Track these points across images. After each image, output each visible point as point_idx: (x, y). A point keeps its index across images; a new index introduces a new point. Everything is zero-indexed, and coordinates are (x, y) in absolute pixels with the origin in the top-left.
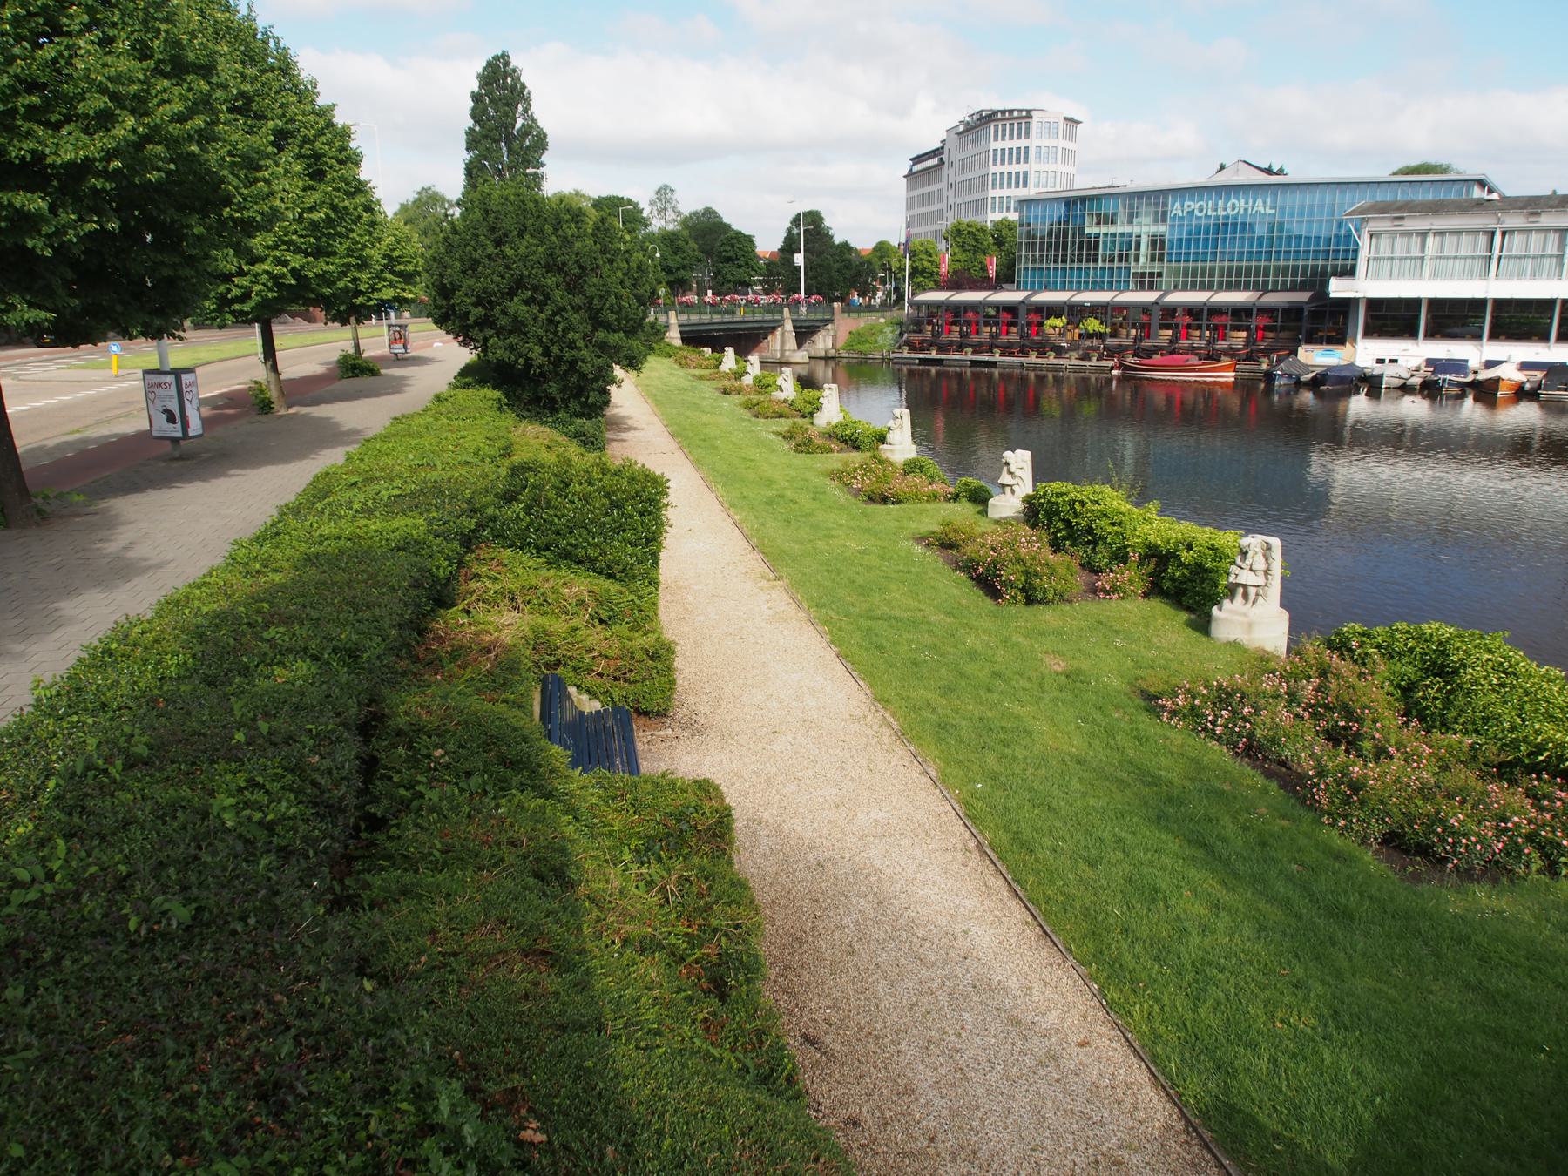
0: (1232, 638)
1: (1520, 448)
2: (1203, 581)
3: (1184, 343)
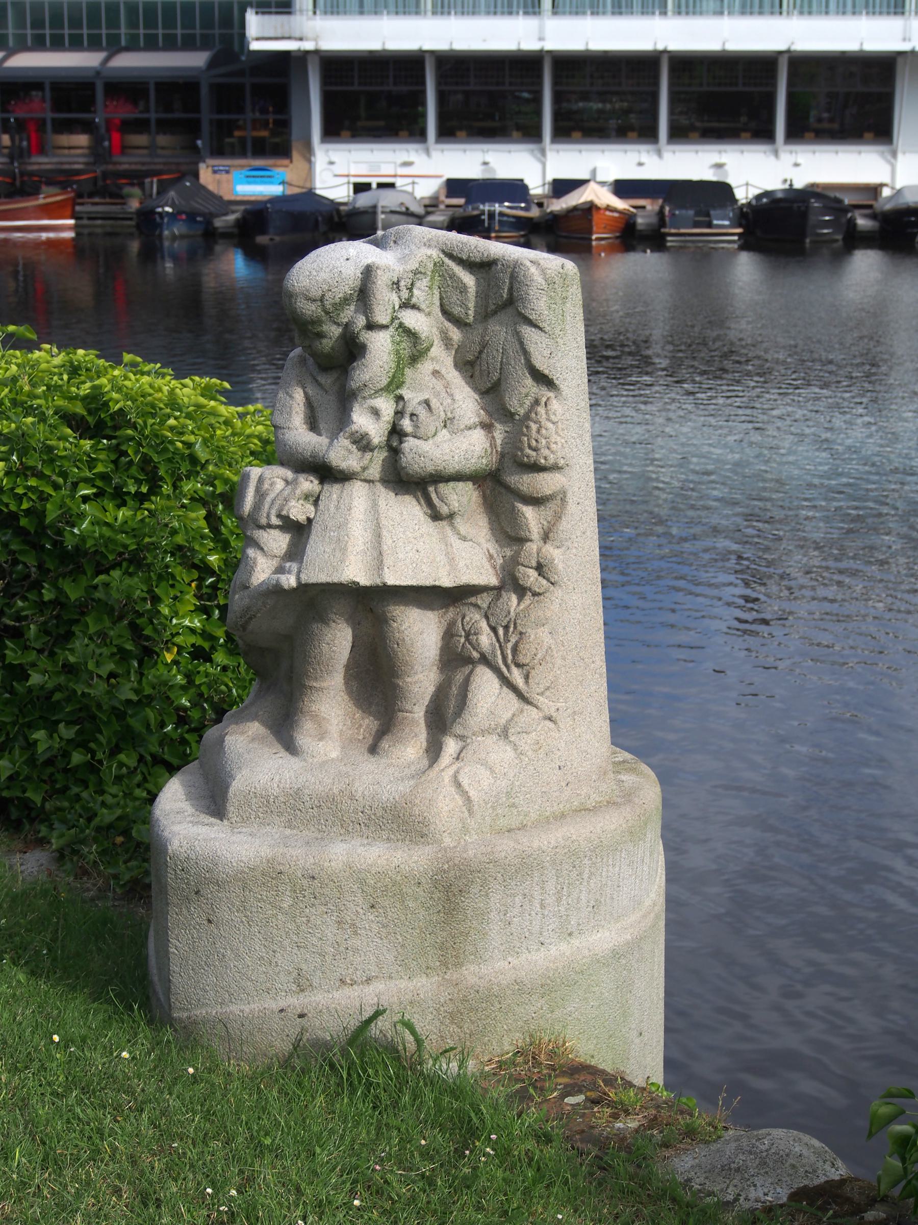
0: (335, 1005)
2: (62, 626)
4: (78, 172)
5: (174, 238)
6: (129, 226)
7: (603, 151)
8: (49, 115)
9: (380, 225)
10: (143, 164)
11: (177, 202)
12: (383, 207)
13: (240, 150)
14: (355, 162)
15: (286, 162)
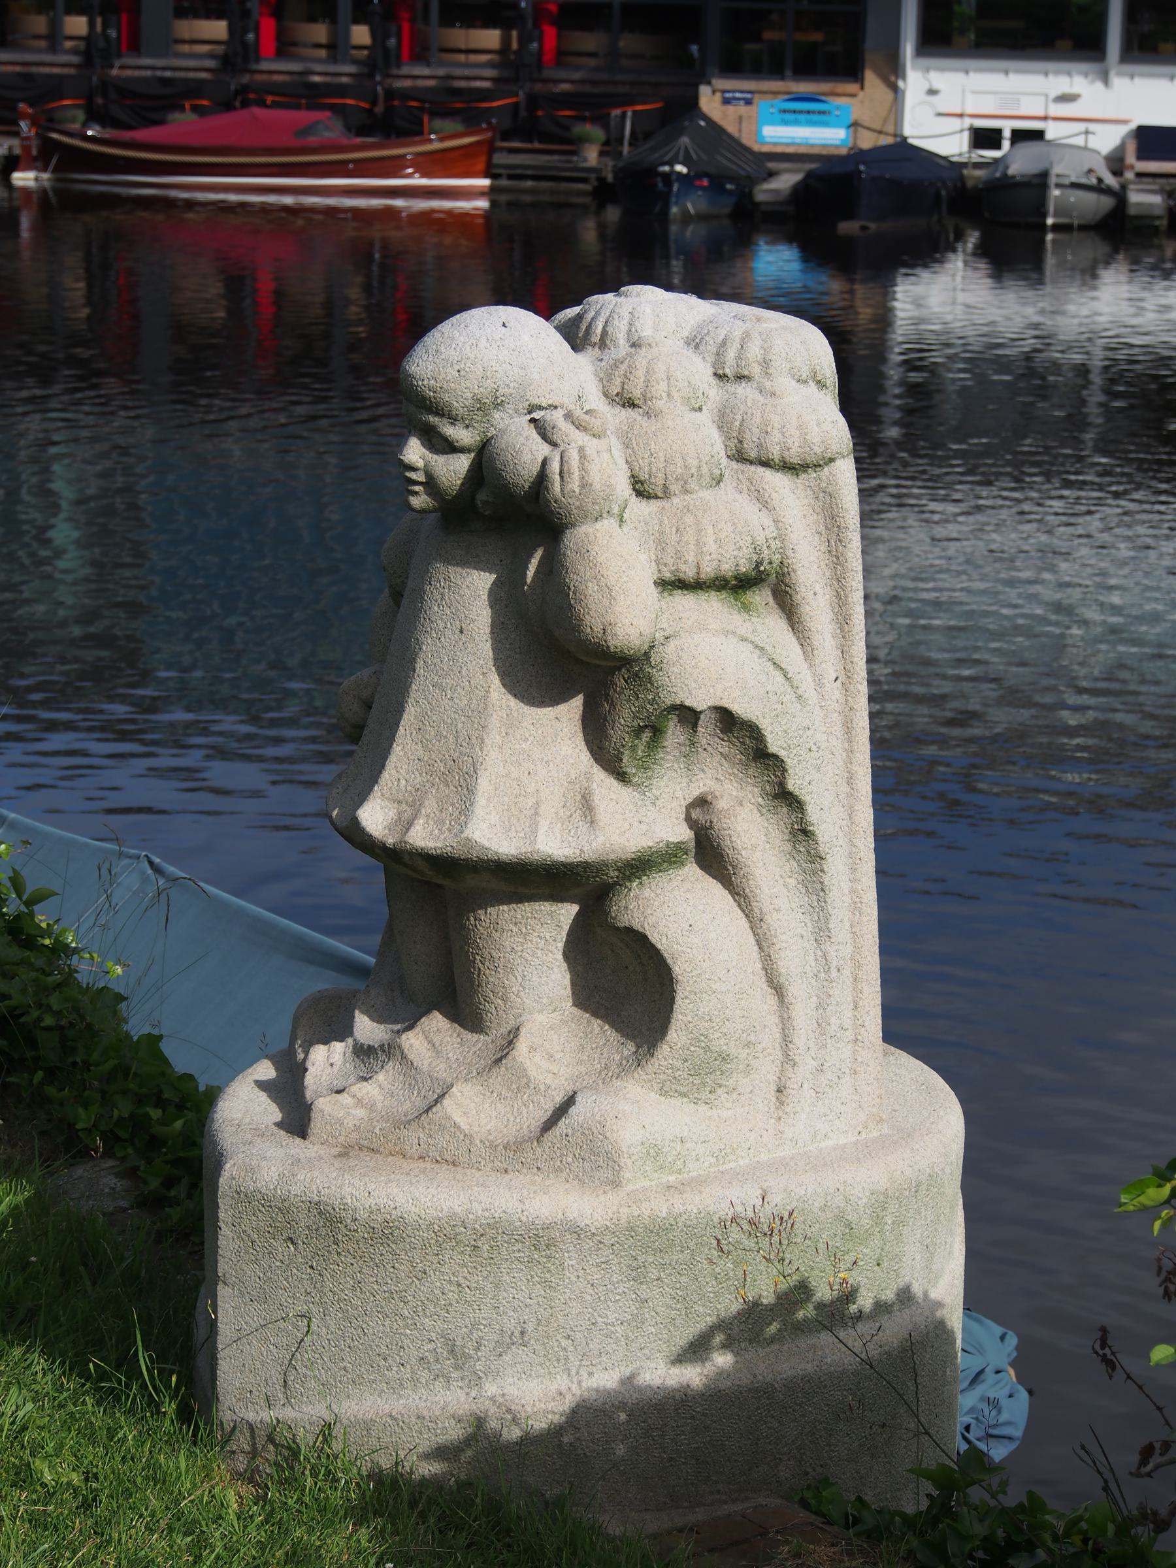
1: (961, 474)
3: (275, 68)
4: (485, 95)
5: (686, 219)
7: (1132, 77)
9: (1051, 209)
10: (594, 83)
11: (694, 157)
12: (1058, 176)
14: (974, 92)
15: (852, 87)
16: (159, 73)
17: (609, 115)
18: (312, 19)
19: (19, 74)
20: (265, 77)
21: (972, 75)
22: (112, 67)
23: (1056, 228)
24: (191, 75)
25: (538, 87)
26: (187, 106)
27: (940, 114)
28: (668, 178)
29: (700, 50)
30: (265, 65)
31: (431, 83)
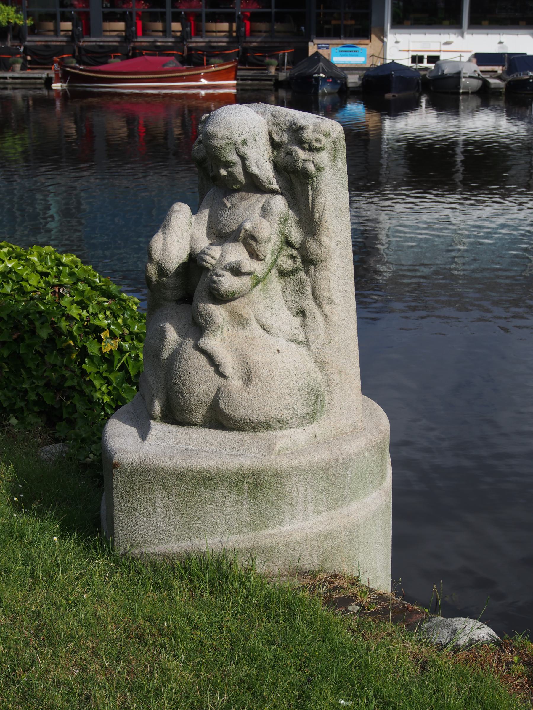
3: (143, 40)
5: (324, 94)
6: (269, 85)
7: (425, 34)
8: (204, 11)
10: (265, 42)
13: (334, 33)
14: (413, 42)
15: (367, 41)
16: (98, 43)
17: (278, 54)
18: (155, 21)
19: (44, 45)
20: (139, 44)
21: (412, 35)
22: (80, 42)
23: (463, 93)
24: (110, 44)
25: (245, 45)
26: (112, 56)
27: (400, 51)
28: (317, 79)
29: (305, 29)
30: (139, 39)
31: (203, 44)
